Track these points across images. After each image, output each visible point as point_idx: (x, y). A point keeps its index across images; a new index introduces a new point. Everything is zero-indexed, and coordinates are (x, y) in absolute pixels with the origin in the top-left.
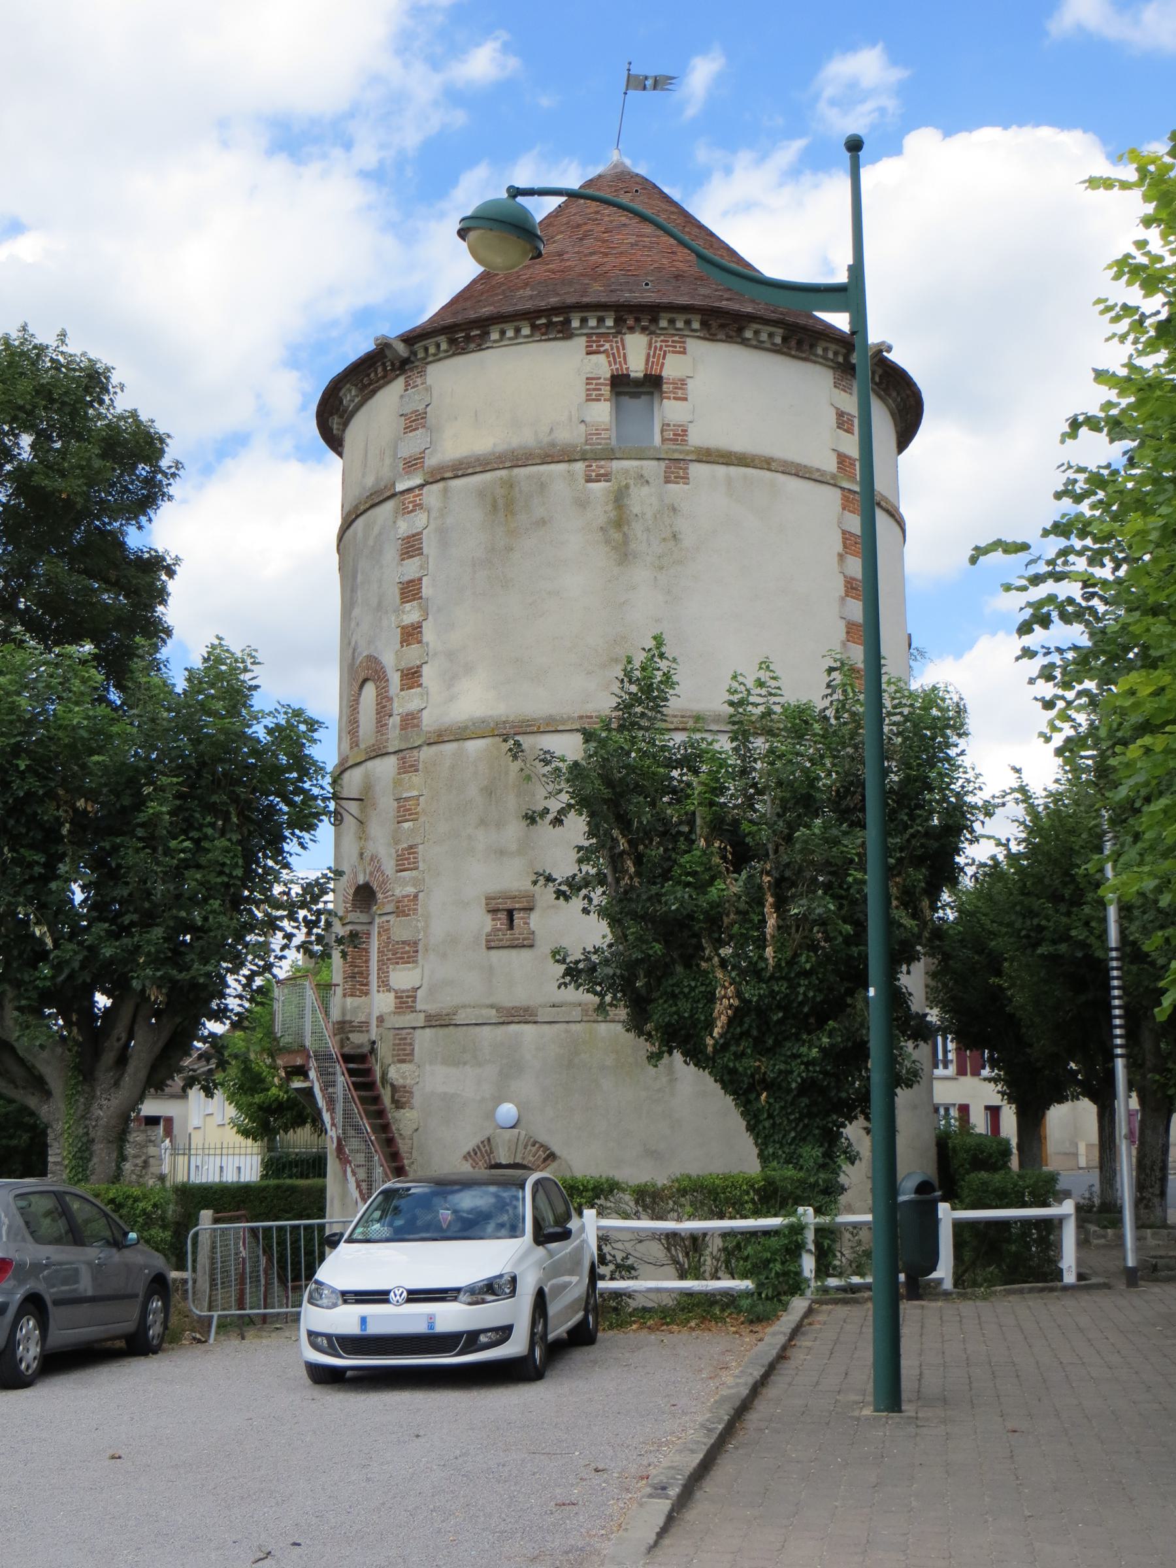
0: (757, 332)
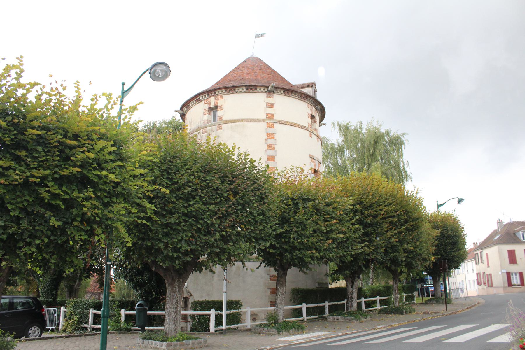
0: (239, 90)
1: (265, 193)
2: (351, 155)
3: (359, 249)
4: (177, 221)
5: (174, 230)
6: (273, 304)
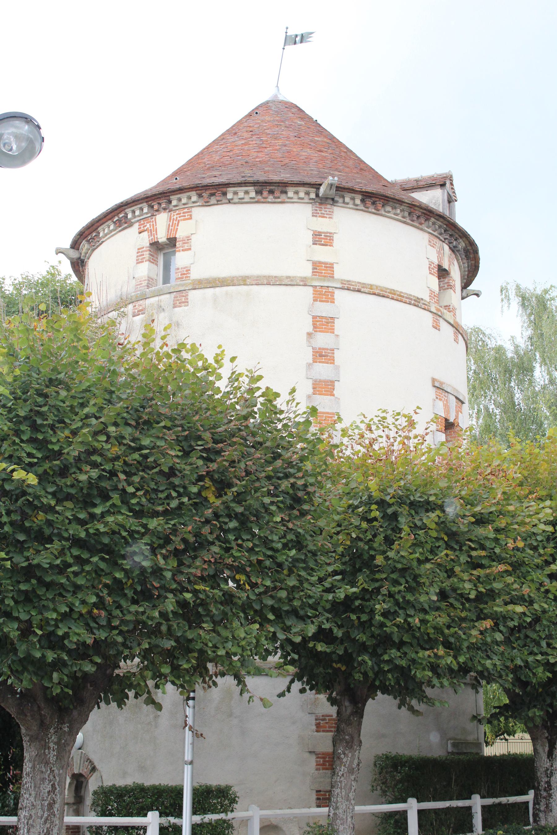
0: (236, 193)
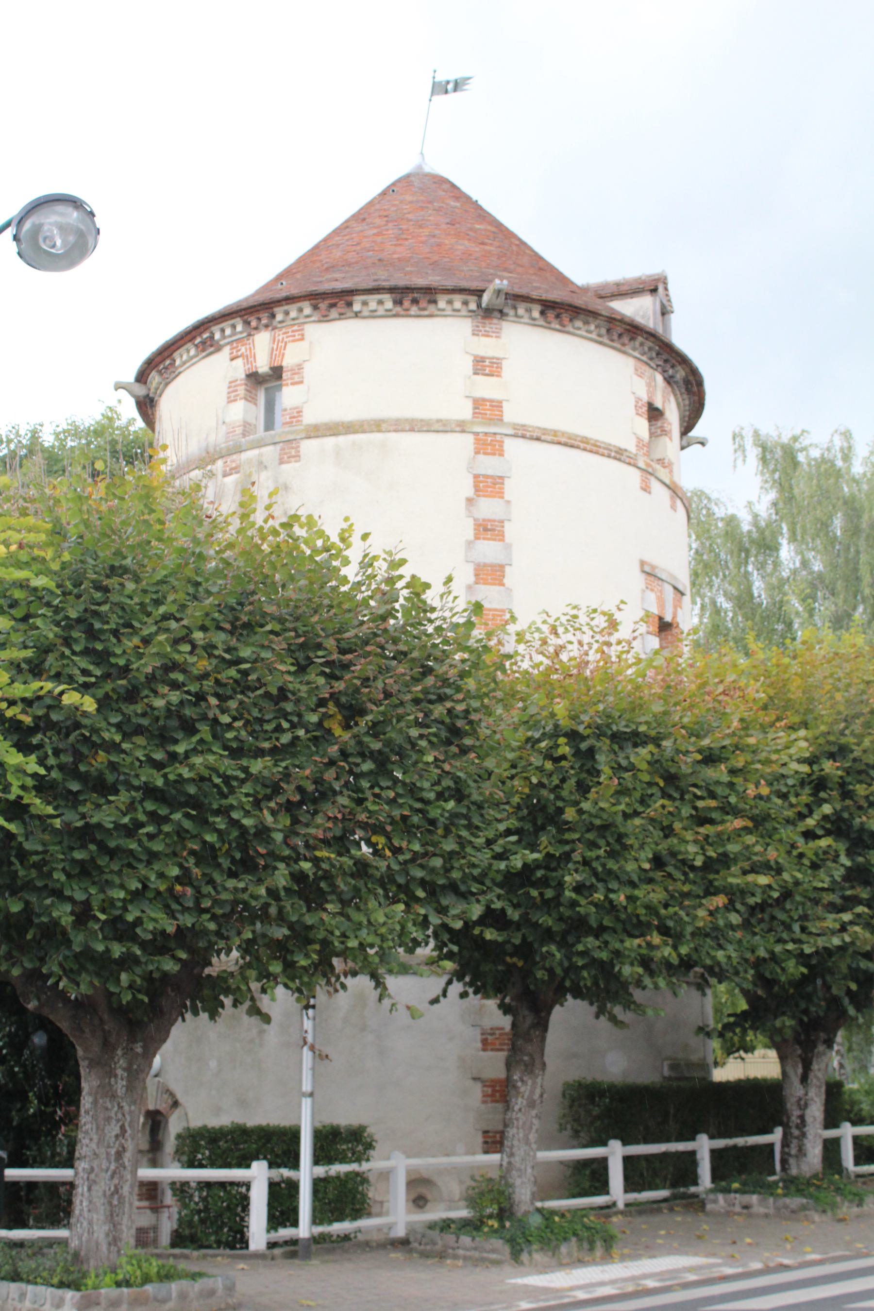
0: (365, 303)
1: (467, 712)
2: (805, 564)
3: (833, 933)
4: (126, 820)
5: (112, 853)
6: (494, 1141)
